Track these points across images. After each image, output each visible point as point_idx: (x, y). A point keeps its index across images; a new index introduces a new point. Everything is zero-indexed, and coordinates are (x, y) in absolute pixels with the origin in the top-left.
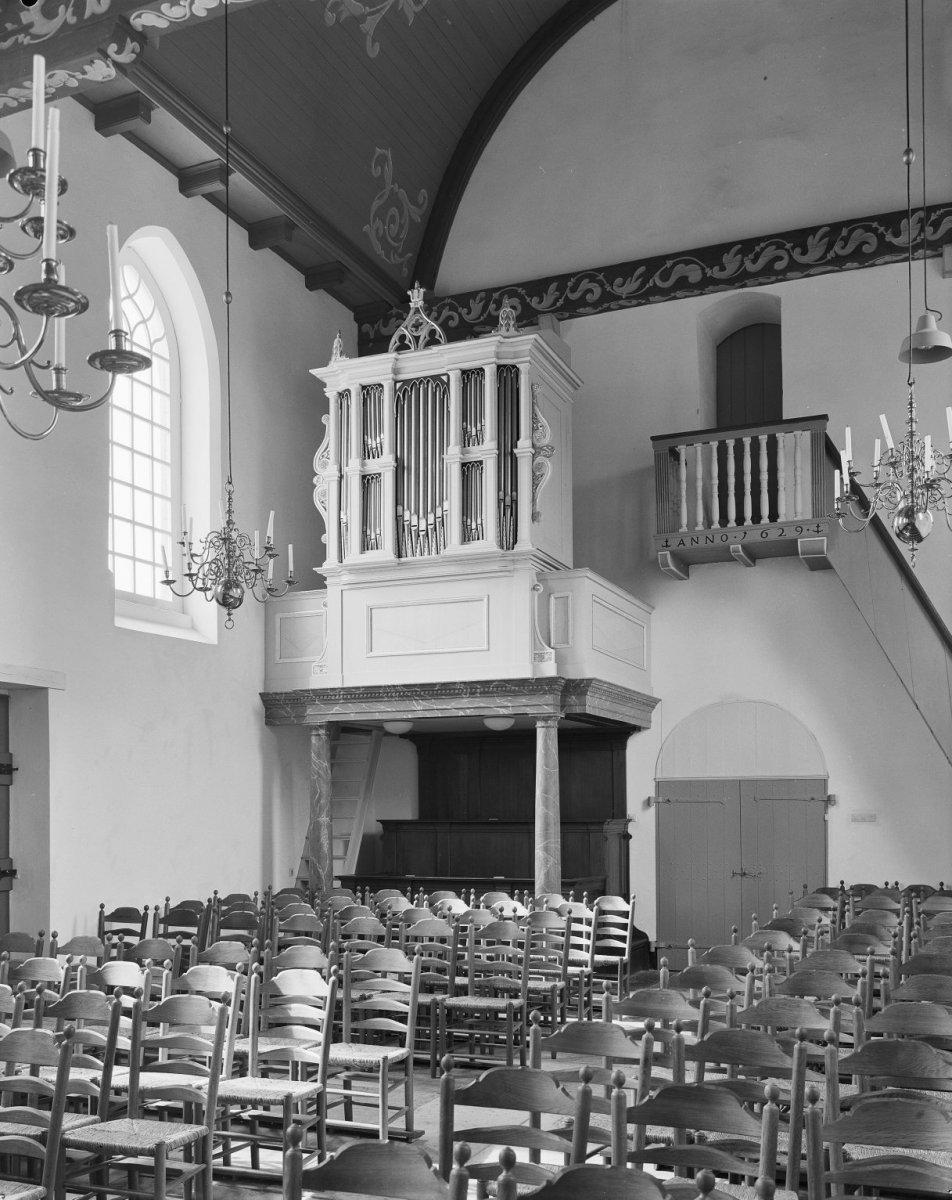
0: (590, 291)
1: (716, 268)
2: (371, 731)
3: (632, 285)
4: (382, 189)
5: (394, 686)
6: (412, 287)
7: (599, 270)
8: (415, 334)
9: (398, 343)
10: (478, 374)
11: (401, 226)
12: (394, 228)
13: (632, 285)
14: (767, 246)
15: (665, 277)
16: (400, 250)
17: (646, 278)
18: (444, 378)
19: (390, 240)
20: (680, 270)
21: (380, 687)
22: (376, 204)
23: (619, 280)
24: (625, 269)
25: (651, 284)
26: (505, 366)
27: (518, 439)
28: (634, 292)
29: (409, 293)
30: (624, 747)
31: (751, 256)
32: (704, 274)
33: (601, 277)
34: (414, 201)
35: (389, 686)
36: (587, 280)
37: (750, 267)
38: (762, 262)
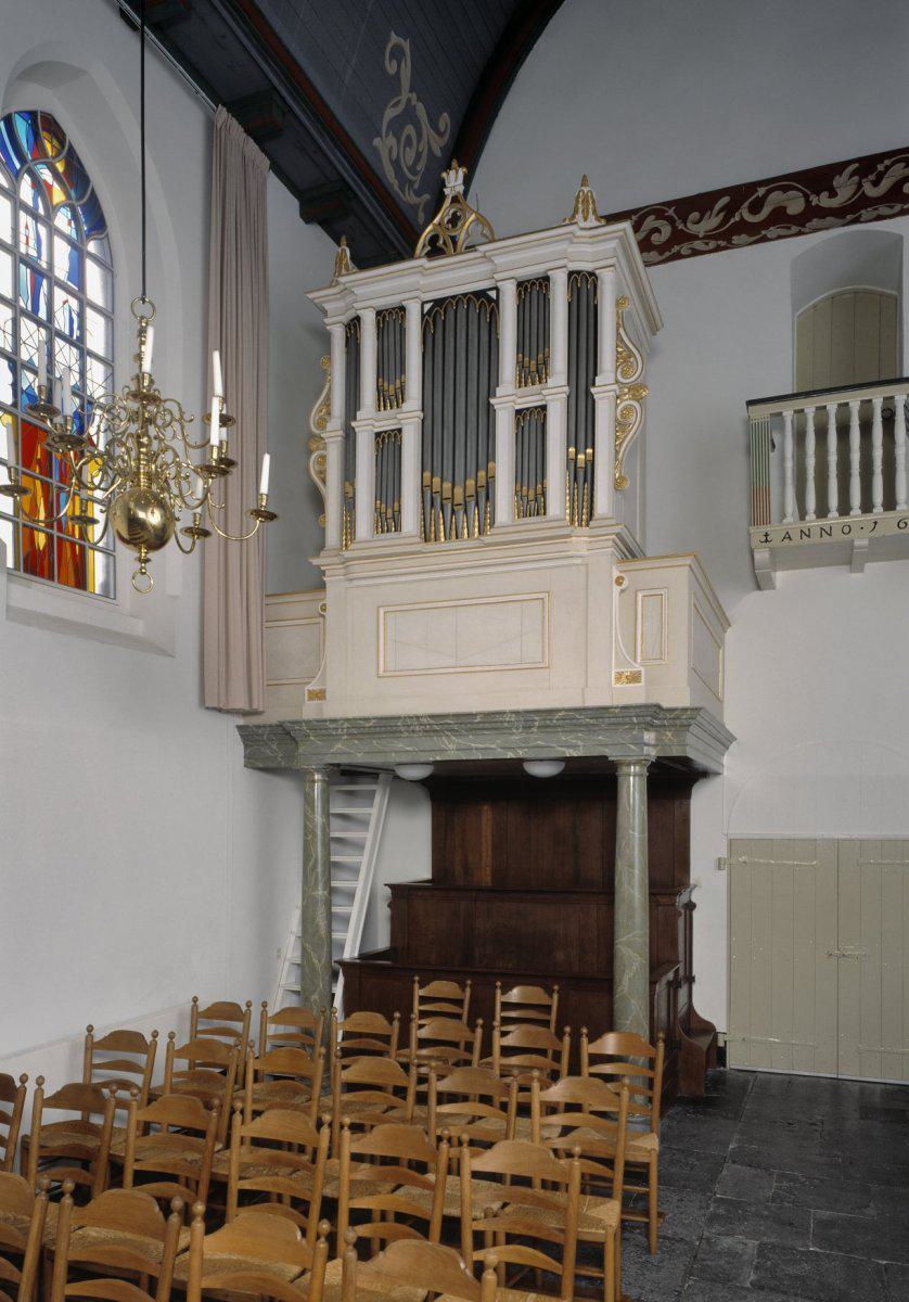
0: (657, 230)
1: (825, 195)
2: (377, 775)
3: (712, 222)
4: (397, 95)
5: (417, 717)
6: (448, 167)
7: (669, 204)
8: (458, 205)
9: (428, 248)
10: (540, 284)
11: (419, 155)
12: (410, 155)
13: (712, 222)
14: (893, 164)
15: (756, 208)
16: (416, 186)
17: (730, 210)
18: (493, 294)
19: (405, 169)
20: (776, 198)
21: (399, 718)
22: (390, 113)
23: (695, 215)
24: (701, 203)
25: (737, 218)
26: (578, 272)
27: (595, 374)
28: (714, 230)
29: (444, 175)
30: (688, 796)
31: (872, 177)
32: (808, 202)
33: (671, 212)
34: (434, 125)
35: (410, 717)
36: (653, 217)
37: (871, 191)
38: (886, 184)
